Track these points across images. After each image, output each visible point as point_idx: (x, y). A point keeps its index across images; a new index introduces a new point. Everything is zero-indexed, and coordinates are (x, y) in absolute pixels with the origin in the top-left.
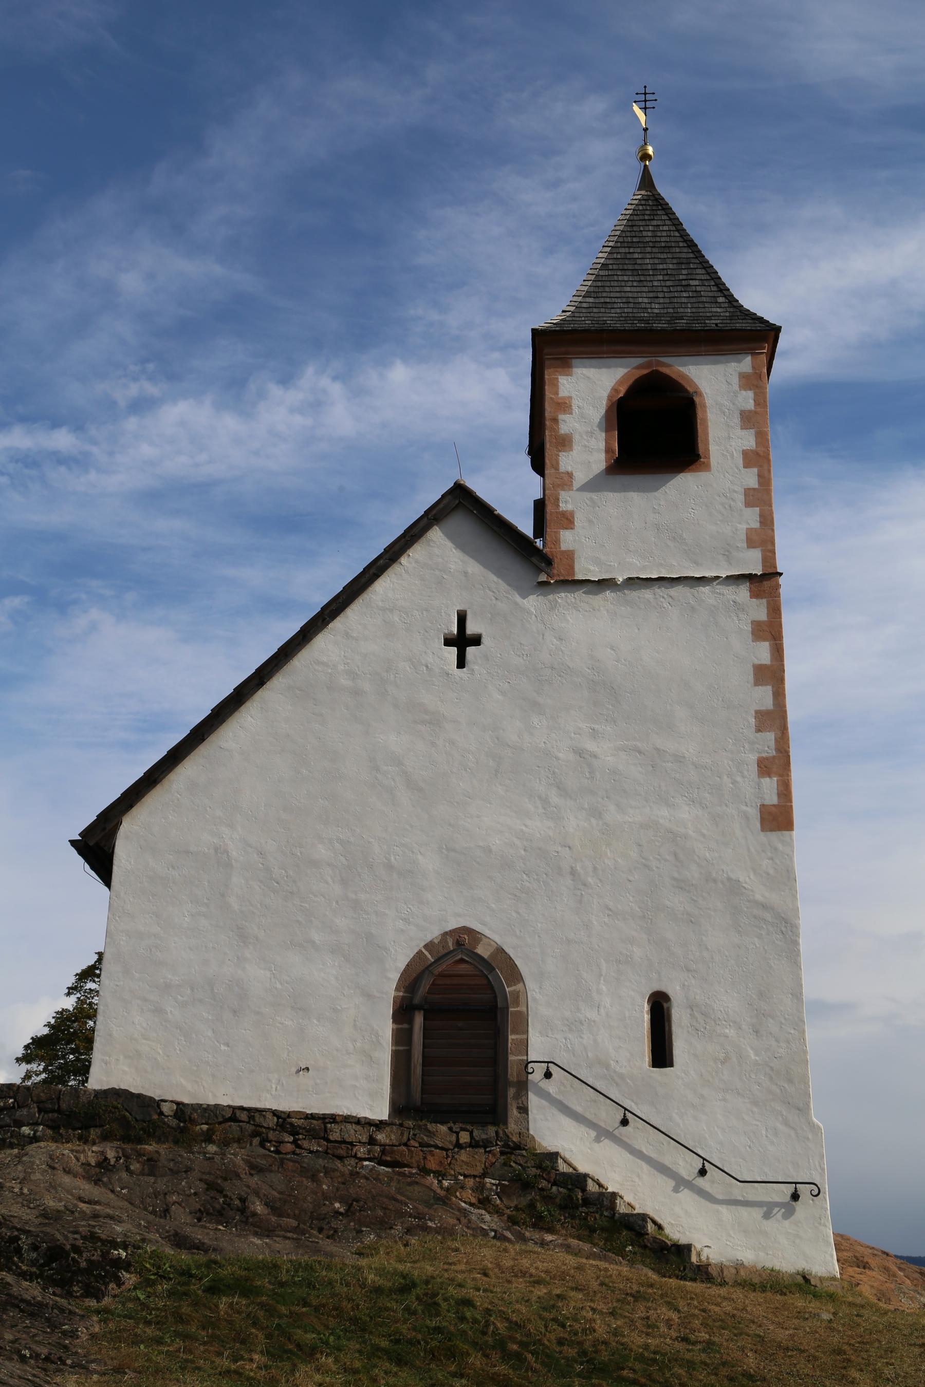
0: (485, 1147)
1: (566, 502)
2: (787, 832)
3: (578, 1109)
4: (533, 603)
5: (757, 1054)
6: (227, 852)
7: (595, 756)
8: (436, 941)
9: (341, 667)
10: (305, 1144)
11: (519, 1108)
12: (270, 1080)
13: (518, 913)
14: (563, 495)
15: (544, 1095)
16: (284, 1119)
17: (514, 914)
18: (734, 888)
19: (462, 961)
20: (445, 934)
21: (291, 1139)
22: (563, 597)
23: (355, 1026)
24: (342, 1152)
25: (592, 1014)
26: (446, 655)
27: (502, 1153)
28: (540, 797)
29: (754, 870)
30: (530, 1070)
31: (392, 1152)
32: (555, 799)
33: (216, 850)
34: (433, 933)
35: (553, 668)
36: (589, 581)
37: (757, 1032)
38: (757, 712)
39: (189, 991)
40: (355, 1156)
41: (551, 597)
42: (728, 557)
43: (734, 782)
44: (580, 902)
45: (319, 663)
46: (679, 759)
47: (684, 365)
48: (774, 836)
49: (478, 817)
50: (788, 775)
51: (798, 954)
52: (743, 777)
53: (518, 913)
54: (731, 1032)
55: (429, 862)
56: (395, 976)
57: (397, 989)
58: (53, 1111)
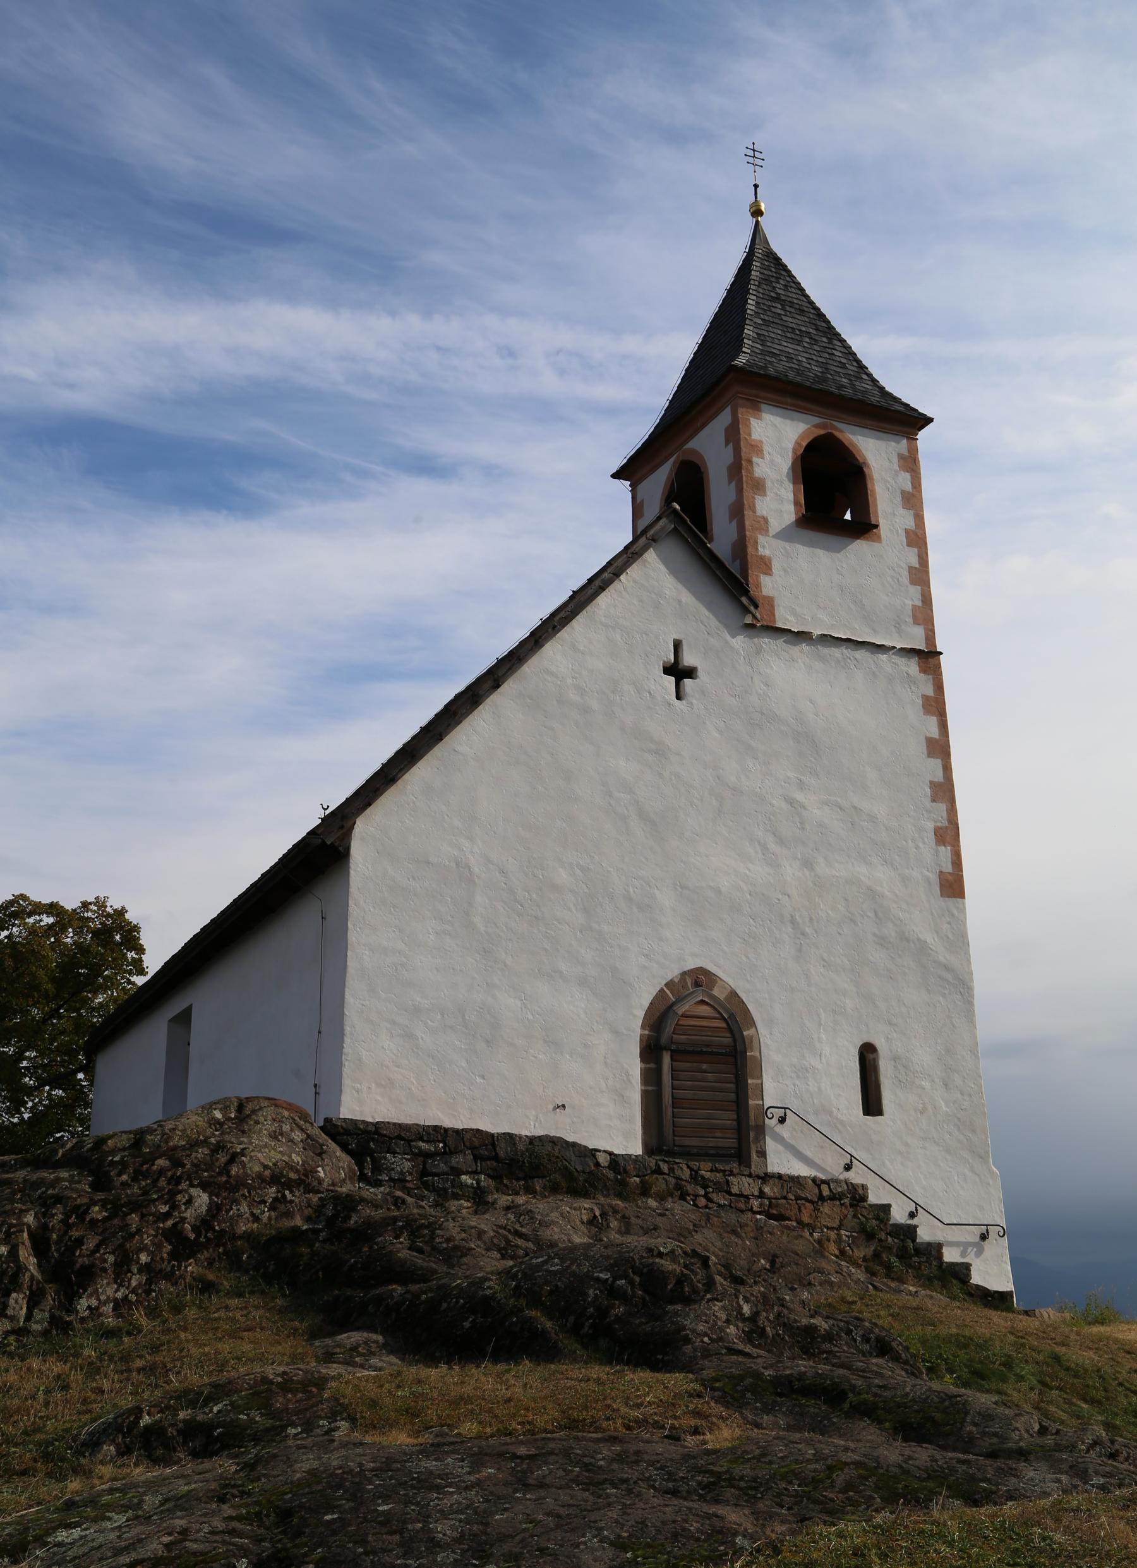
0: (840, 1200)
1: (764, 547)
2: (959, 900)
3: (809, 1154)
4: (740, 642)
5: (947, 1106)
6: (469, 867)
7: (804, 808)
8: (676, 980)
9: (569, 681)
10: (714, 1197)
11: (757, 1152)
12: (527, 1117)
13: (747, 957)
14: (761, 539)
15: (780, 1139)
16: (696, 1172)
17: (744, 959)
18: (922, 948)
19: (702, 1002)
20: (684, 973)
21: (702, 1192)
22: (767, 642)
23: (606, 1063)
24: (742, 1206)
25: (814, 1062)
26: (666, 684)
27: (851, 1205)
28: (759, 842)
29: (937, 933)
30: (770, 1116)
31: (777, 1205)
32: (773, 846)
33: (457, 864)
34: (673, 972)
35: (762, 714)
36: (789, 631)
37: (946, 1085)
38: (931, 782)
39: (439, 1017)
40: (751, 1210)
41: (756, 640)
42: (899, 631)
43: (917, 848)
44: (800, 950)
45: (548, 672)
46: (873, 819)
47: (854, 434)
48: (951, 902)
49: (707, 856)
50: (959, 846)
51: (974, 1015)
52: (924, 843)
53: (747, 957)
54: (926, 1084)
55: (666, 898)
56: (641, 1014)
57: (643, 1027)
58: (489, 1159)
